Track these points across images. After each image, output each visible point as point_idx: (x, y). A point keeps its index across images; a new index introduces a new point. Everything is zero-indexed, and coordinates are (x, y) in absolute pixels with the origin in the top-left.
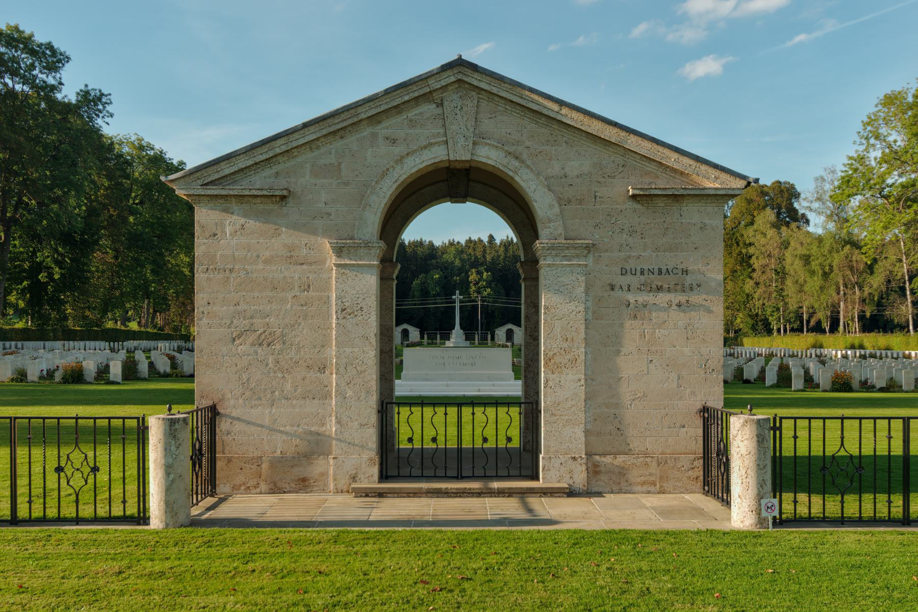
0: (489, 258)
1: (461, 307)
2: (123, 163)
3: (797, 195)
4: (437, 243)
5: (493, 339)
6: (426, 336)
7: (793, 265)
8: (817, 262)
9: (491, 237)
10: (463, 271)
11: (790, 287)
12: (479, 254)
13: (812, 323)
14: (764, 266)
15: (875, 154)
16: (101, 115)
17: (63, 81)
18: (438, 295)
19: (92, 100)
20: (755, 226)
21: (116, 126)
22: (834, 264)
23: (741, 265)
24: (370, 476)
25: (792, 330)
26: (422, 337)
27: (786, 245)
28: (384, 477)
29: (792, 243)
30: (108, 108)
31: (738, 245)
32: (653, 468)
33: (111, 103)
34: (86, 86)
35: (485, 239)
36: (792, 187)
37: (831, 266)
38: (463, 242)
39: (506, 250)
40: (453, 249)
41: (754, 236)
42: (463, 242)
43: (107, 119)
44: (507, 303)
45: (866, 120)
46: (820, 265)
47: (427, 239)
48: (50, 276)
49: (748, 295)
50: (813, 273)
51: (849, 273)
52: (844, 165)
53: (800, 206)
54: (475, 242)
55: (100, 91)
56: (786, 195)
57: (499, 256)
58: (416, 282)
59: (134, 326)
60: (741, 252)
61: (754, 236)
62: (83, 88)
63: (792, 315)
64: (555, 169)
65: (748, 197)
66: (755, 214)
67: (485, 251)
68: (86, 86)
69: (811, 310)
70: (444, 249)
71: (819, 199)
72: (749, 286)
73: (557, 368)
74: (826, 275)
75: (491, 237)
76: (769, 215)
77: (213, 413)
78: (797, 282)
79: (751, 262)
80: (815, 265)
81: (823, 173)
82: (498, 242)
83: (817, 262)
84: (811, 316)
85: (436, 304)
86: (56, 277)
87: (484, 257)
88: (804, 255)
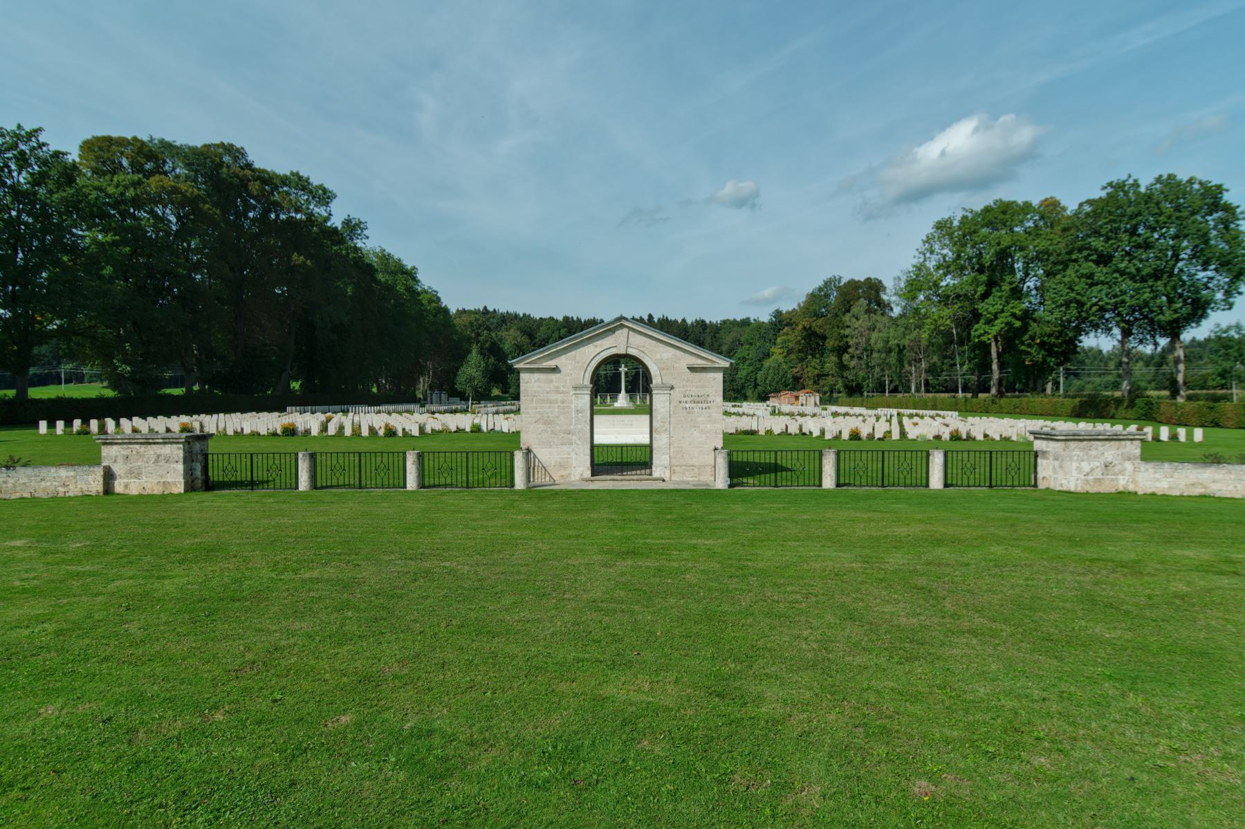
2: (369, 270)
14: (857, 344)
15: (931, 264)
19: (353, 227)
24: (588, 474)
28: (593, 475)
30: (365, 232)
32: (696, 471)
36: (880, 282)
64: (658, 356)
73: (660, 433)
77: (529, 451)
81: (899, 274)
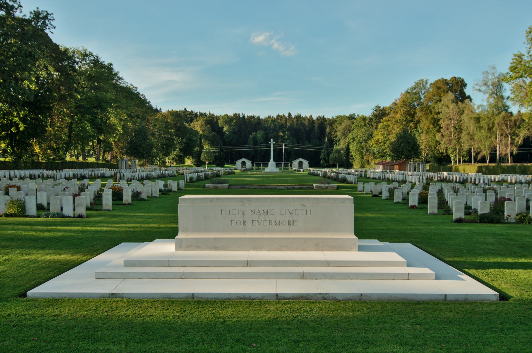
0: (288, 124)
1: (274, 150)
3: (465, 85)
4: (262, 117)
5: (291, 166)
6: (255, 165)
7: (469, 125)
8: (485, 122)
9: (290, 114)
10: (275, 130)
11: (464, 137)
12: (283, 122)
13: (479, 157)
16: (47, 27)
17: (21, 4)
18: (262, 143)
20: (442, 102)
21: (60, 36)
22: (496, 123)
23: (433, 125)
25: (464, 161)
26: (253, 165)
27: (462, 112)
29: (466, 112)
30: (53, 23)
31: (431, 114)
33: (54, 19)
34: (38, 8)
35: (287, 115)
37: (493, 124)
38: (275, 117)
39: (297, 120)
40: (270, 119)
41: (441, 108)
42: (275, 117)
43: (52, 30)
44: (298, 147)
45: (528, 30)
46: (486, 123)
47: (257, 115)
48: (18, 128)
49: (437, 142)
50: (481, 128)
51: (504, 127)
52: (513, 59)
53: (468, 91)
54: (281, 116)
55: (46, 12)
56: (460, 84)
57: (294, 123)
58: (251, 136)
59: (92, 160)
60: (434, 117)
61: (441, 108)
62: (36, 10)
63: (465, 153)
65: (438, 86)
66: (442, 95)
67: (286, 121)
68: (38, 8)
69: (479, 150)
70: (266, 120)
71: (485, 84)
72: (438, 136)
74: (490, 129)
75: (290, 114)
76: (451, 96)
78: (469, 134)
79: (439, 123)
80: (483, 123)
82: (293, 116)
83: (485, 122)
84: (477, 154)
85: (261, 148)
86: (21, 129)
87: (286, 124)
88: (476, 118)
